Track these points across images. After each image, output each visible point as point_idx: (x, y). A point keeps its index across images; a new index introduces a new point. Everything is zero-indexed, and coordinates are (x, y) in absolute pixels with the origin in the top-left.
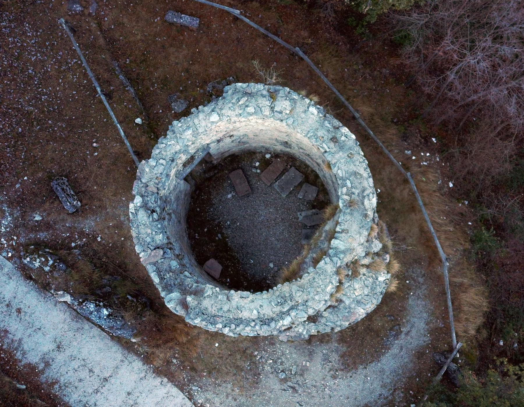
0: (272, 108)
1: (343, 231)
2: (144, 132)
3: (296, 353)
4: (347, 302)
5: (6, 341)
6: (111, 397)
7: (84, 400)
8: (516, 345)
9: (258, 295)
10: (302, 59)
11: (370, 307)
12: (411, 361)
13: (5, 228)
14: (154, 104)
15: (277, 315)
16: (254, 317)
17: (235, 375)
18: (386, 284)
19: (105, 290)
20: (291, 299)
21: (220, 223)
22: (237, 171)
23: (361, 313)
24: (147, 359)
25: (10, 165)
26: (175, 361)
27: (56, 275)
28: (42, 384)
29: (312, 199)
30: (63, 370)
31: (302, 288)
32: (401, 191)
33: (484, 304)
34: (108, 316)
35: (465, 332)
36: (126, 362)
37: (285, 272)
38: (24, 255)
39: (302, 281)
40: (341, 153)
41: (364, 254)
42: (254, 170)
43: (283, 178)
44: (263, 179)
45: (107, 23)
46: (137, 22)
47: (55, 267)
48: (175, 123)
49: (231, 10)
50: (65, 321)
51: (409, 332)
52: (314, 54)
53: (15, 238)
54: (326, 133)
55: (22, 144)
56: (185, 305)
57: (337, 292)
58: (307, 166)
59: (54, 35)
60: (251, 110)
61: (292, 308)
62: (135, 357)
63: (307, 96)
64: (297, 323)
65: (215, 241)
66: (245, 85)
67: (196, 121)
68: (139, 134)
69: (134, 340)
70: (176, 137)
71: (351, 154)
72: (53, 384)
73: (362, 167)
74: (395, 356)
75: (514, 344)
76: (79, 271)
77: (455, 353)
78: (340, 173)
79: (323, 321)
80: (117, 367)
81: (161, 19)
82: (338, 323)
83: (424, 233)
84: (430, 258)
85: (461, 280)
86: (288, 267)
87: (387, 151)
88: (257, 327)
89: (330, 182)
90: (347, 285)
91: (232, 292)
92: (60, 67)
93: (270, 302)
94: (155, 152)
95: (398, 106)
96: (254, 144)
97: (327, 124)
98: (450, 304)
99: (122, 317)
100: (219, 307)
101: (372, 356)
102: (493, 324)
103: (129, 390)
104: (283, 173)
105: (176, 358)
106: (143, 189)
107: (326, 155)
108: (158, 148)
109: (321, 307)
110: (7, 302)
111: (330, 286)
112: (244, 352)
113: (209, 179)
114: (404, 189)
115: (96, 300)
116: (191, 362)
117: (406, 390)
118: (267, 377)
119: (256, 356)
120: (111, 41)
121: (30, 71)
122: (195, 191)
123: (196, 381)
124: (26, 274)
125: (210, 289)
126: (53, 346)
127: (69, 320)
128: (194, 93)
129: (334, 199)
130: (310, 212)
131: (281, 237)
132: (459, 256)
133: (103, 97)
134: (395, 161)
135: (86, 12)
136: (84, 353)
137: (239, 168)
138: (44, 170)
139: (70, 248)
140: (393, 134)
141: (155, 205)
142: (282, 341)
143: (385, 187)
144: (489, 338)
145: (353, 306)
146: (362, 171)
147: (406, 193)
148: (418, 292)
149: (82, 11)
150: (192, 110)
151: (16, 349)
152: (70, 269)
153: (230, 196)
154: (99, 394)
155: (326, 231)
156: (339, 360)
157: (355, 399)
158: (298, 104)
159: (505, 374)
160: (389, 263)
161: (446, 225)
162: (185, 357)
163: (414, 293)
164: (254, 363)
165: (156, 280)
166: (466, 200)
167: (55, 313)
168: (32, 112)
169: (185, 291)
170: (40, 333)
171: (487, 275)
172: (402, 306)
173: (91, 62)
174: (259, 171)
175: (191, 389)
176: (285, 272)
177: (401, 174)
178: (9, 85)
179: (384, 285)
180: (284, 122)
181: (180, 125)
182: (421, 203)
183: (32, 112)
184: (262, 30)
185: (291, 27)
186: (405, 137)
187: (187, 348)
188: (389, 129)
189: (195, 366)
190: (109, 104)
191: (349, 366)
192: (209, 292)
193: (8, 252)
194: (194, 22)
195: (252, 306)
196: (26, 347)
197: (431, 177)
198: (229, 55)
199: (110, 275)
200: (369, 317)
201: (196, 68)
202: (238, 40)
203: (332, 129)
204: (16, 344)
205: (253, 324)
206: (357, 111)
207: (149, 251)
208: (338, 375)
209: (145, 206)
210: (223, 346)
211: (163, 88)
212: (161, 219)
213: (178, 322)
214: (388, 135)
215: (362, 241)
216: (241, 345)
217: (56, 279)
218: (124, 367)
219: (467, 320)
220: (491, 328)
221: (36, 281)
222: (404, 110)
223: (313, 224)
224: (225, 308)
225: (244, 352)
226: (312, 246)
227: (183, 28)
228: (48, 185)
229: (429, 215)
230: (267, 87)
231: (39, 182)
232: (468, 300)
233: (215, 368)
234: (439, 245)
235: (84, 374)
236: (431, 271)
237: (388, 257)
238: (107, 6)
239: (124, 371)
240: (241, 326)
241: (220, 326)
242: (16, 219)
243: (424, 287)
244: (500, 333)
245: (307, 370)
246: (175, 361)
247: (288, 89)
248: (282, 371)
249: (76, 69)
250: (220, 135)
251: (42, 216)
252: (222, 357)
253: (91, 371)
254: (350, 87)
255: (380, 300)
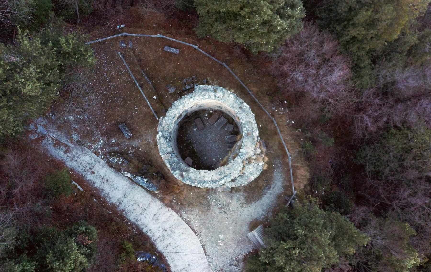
0: (215, 96)
1: (245, 145)
2: (157, 102)
3: (225, 197)
4: (247, 174)
5: (103, 193)
6: (147, 216)
7: (136, 218)
8: (323, 193)
9: (211, 171)
10: (225, 67)
11: (256, 176)
12: (275, 200)
13: (100, 146)
14: (160, 89)
15: (219, 179)
16: (210, 180)
17: (199, 206)
18: (263, 166)
19: (144, 171)
20: (224, 172)
21: (191, 141)
22: (198, 119)
23: (252, 178)
24: (162, 200)
25: (100, 118)
26: (174, 201)
27: (124, 165)
28: (118, 211)
29: (231, 130)
30: (127, 205)
31: (229, 169)
32: (271, 126)
33: (308, 175)
34: (147, 182)
35: (299, 187)
36: (153, 202)
37: (222, 162)
38: (110, 157)
39: (229, 166)
40: (243, 114)
41: (253, 155)
42: (205, 118)
43: (218, 121)
44: (210, 122)
45: (137, 52)
46: (151, 51)
47: (123, 162)
48: (175, 102)
49: (194, 46)
50: (127, 184)
51: (274, 187)
52: (231, 64)
53: (104, 150)
54: (237, 105)
55: (104, 109)
56: (182, 176)
57: (243, 169)
58: (229, 116)
59: (115, 58)
60: (206, 97)
61: (225, 176)
62: (157, 200)
63: (229, 90)
64: (227, 182)
65: (189, 149)
66: (204, 86)
67: (184, 101)
68: (155, 103)
69: (156, 192)
70: (176, 108)
71: (248, 114)
72: (123, 211)
73: (253, 121)
74: (268, 198)
75: (322, 193)
76: (133, 163)
77: (293, 196)
78: (243, 122)
79: (237, 181)
80: (149, 204)
81: (161, 49)
82: (243, 182)
83: (280, 144)
84: (283, 155)
85: (297, 164)
86: (222, 160)
87: (264, 109)
88: (211, 184)
89: (239, 124)
90: (246, 167)
91: (201, 170)
92: (118, 73)
93: (216, 174)
94: (167, 114)
95: (269, 86)
96: (205, 107)
97: (237, 101)
98: (292, 175)
99: (152, 183)
100: (196, 176)
101: (258, 198)
102: (313, 184)
103: (155, 213)
104: (218, 119)
105: (174, 200)
106: (162, 129)
107: (237, 114)
108: (168, 113)
109: (236, 176)
110: (102, 177)
111: (240, 167)
112: (203, 196)
113: (186, 122)
114: (272, 125)
115: (141, 176)
116: (181, 201)
117: (273, 212)
118: (213, 206)
119: (208, 198)
120: (140, 60)
121: (105, 75)
122: (180, 128)
123: (183, 209)
124: (110, 165)
125: (192, 169)
126: (122, 195)
127: (128, 184)
128: (178, 84)
129: (241, 133)
130: (230, 136)
131: (218, 147)
132: (296, 154)
133: (139, 88)
134: (268, 113)
135: (128, 47)
136: (136, 198)
137: (199, 117)
138: (115, 120)
139: (128, 154)
140: (267, 100)
141: (167, 135)
142: (219, 192)
143: (264, 124)
144: (311, 190)
145: (249, 175)
146: (252, 121)
147: (273, 126)
148: (278, 170)
149: (126, 47)
150: (182, 97)
151: (107, 197)
152: (129, 163)
153: (195, 130)
154: (142, 215)
155: (238, 146)
156: (244, 200)
157: (251, 216)
158: (226, 94)
159: (311, 202)
160: (264, 158)
161: (291, 140)
162: (178, 199)
163: (276, 171)
164: (208, 201)
165: (169, 166)
166: (300, 129)
167: (123, 181)
168: (107, 94)
169: (181, 170)
170: (117, 190)
171: (309, 162)
172: (271, 176)
173: (132, 71)
174: (207, 118)
175: (181, 213)
176: (222, 162)
177: (270, 118)
178: (96, 82)
179: (262, 167)
180: (220, 101)
181: (177, 103)
182: (279, 131)
183: (107, 94)
184: (208, 55)
185: (220, 52)
186: (272, 102)
187: (179, 195)
188: (265, 98)
189: (183, 202)
190: (142, 90)
191: (248, 202)
192: (192, 171)
193: (101, 156)
194: (177, 51)
195: (209, 176)
196: (111, 196)
197: (284, 119)
198: (193, 65)
199: (146, 165)
200: (256, 180)
201: (178, 72)
202: (197, 59)
203: (240, 104)
204: (107, 195)
205: (209, 183)
206: (250, 91)
207: (166, 154)
208: (244, 206)
209: (163, 136)
210: (194, 194)
211: (164, 81)
212: (170, 141)
213: (175, 184)
214: (265, 101)
215: (253, 149)
216: (202, 194)
217: (124, 167)
218: (152, 204)
219: (300, 182)
220: (312, 186)
221: (114, 168)
222: (272, 88)
223: (232, 141)
224: (199, 177)
225: (203, 196)
226: (232, 152)
227: (171, 54)
228: (117, 127)
229: (282, 136)
230: (213, 87)
231: (113, 126)
232: (300, 173)
233: (191, 204)
234: (287, 149)
235: (136, 207)
236: (284, 161)
237: (263, 156)
238: (137, 43)
239: (152, 205)
240: (205, 184)
241: (196, 184)
242: (105, 141)
243: (281, 168)
244: (317, 188)
245: (230, 204)
246: (174, 201)
247: (221, 88)
248: (220, 204)
249: (125, 74)
250: (192, 105)
251: (115, 140)
252: (194, 199)
253: (138, 206)
254: (247, 79)
255: (260, 173)
